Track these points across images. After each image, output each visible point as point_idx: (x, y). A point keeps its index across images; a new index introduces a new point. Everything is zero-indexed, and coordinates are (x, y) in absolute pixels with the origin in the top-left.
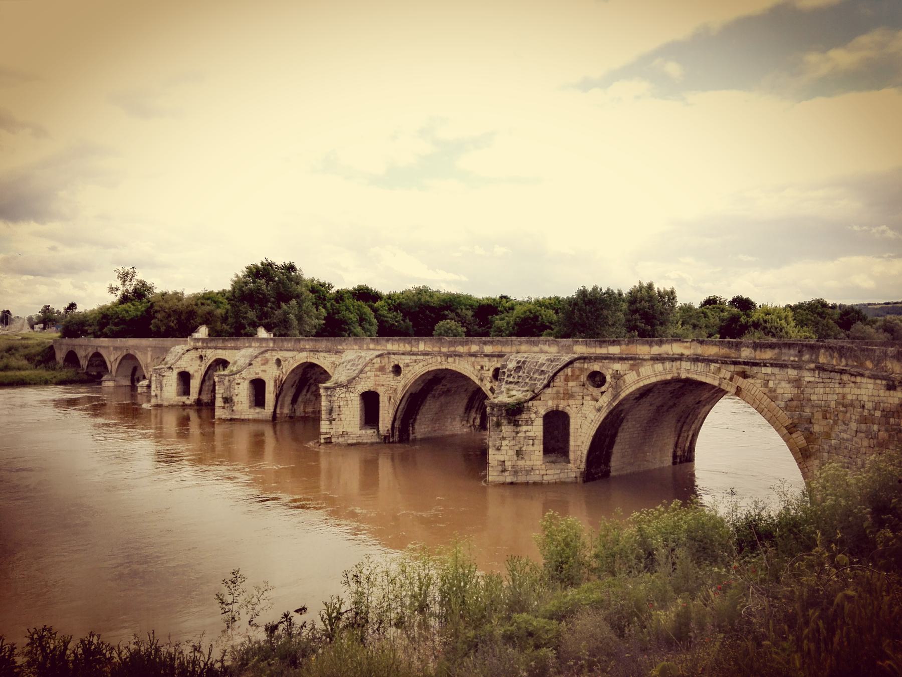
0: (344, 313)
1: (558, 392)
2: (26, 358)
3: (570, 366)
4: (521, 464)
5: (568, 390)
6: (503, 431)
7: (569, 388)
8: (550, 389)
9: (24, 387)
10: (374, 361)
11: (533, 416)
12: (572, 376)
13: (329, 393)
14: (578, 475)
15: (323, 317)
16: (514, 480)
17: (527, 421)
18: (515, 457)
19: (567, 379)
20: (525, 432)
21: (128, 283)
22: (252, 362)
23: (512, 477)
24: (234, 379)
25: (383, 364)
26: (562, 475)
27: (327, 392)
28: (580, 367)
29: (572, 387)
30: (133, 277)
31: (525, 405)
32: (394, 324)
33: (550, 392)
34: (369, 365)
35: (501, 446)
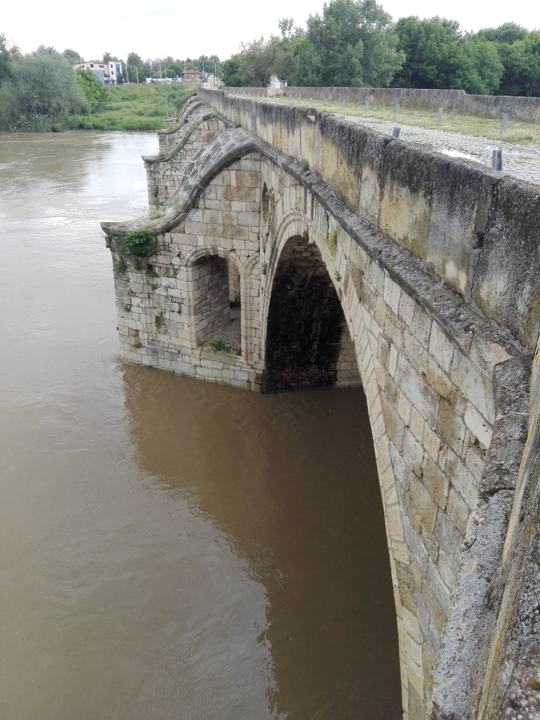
0: (460, 56)
1: (213, 220)
2: (176, 104)
3: (235, 166)
4: (163, 340)
5: (231, 219)
6: (131, 281)
7: (234, 214)
8: (199, 213)
9: (149, 133)
10: (201, 126)
11: (176, 261)
12: (239, 188)
13: (152, 169)
14: (253, 379)
15: (401, 63)
16: (154, 363)
17: (168, 269)
18: (154, 328)
19: (228, 196)
20: (167, 288)
21: (287, 32)
22: (188, 119)
23: (150, 358)
24: (174, 139)
25: (212, 131)
26: (225, 373)
27: (150, 168)
28: (253, 168)
29: (238, 212)
30: (291, 25)
31: (160, 238)
32: (526, 70)
33: (200, 219)
34: (195, 131)
35: (131, 305)
